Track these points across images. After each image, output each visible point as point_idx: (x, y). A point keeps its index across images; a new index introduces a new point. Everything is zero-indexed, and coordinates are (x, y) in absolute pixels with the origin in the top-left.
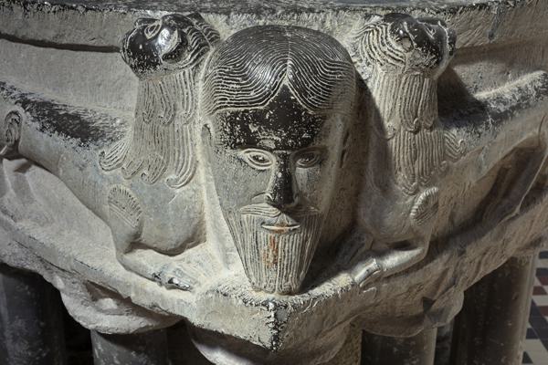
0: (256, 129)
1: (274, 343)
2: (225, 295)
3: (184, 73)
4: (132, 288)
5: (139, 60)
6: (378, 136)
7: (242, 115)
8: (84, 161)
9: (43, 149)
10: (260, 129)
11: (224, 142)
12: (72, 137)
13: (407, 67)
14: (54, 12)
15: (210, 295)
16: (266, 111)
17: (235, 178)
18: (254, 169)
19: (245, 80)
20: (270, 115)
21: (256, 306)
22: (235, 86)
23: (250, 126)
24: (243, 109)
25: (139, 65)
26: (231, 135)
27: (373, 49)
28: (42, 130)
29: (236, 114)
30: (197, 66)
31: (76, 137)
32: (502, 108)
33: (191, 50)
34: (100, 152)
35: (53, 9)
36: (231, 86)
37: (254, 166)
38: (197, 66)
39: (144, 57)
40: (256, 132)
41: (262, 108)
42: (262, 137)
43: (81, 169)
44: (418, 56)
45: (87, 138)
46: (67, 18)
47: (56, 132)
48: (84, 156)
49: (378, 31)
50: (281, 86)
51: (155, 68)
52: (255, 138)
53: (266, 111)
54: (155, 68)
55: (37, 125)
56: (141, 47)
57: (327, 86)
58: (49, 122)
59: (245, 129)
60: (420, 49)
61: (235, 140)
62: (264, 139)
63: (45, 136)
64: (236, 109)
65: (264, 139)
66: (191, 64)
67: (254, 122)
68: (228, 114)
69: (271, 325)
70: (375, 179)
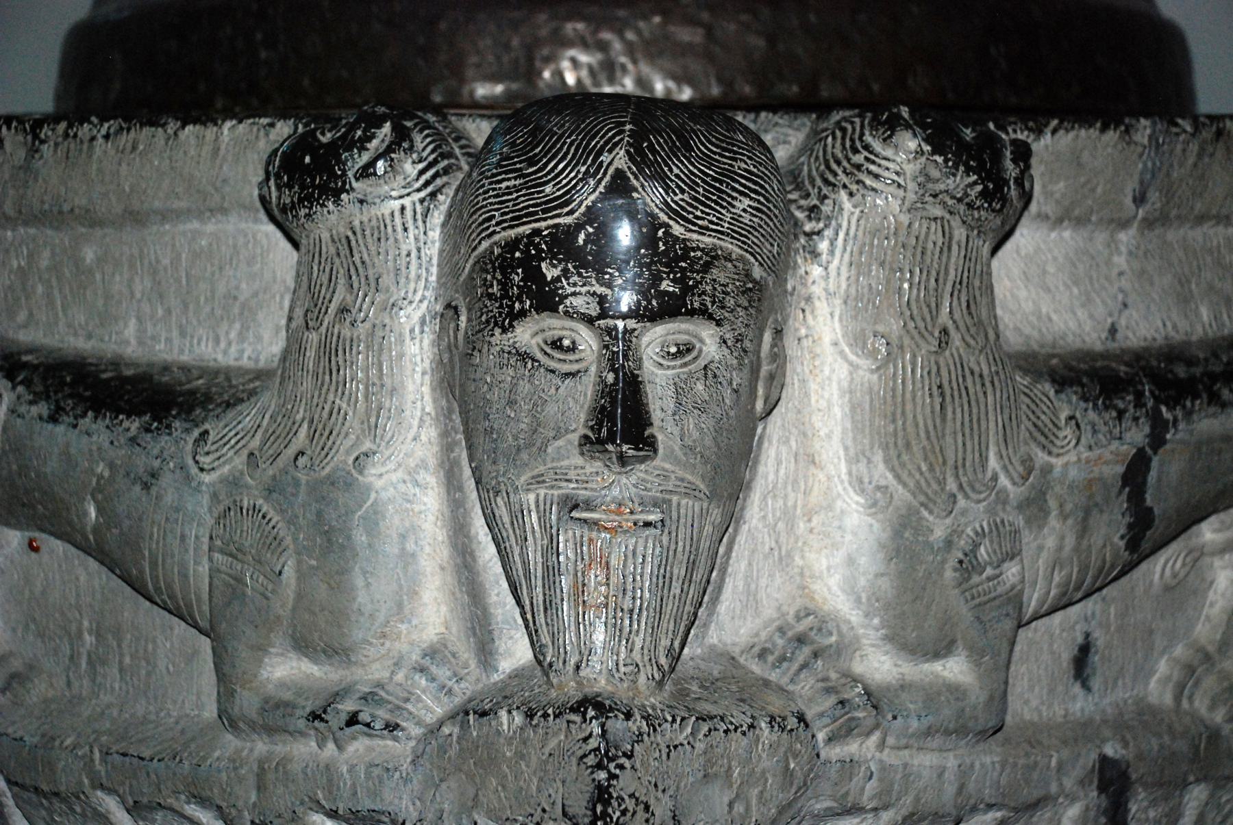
0: (556, 272)
1: (599, 808)
2: (484, 714)
3: (403, 208)
4: (238, 304)
5: (303, 187)
6: (851, 364)
7: (527, 246)
8: (157, 463)
9: (52, 466)
10: (565, 272)
11: (488, 322)
12: (129, 417)
13: (911, 196)
14: (107, 137)
15: (446, 730)
16: (579, 227)
17: (511, 403)
18: (553, 372)
19: (531, 165)
20: (588, 235)
21: (556, 716)
22: (513, 182)
23: (543, 265)
24: (526, 229)
25: (301, 200)
26: (502, 298)
27: (834, 166)
28: (53, 419)
29: (512, 245)
30: (433, 195)
31: (139, 414)
32: (1181, 371)
33: (420, 161)
34: (196, 433)
35: (103, 131)
36: (504, 185)
37: (553, 365)
38: (433, 195)
39: (314, 180)
40: (558, 279)
41: (568, 220)
42: (570, 290)
43: (146, 487)
44: (935, 174)
45: (168, 410)
46: (134, 148)
47: (90, 414)
48: (156, 452)
49: (844, 130)
50: (610, 172)
51: (337, 202)
52: (554, 292)
53: (579, 227)
54: (337, 202)
55: (43, 409)
56: (307, 159)
57: (714, 179)
58: (71, 396)
59: (534, 275)
60: (940, 159)
61: (512, 307)
62: (574, 294)
63: (60, 429)
64: (512, 233)
65: (574, 294)
66: (419, 190)
67: (554, 257)
68: (497, 251)
69: (591, 760)
70: (850, 473)
